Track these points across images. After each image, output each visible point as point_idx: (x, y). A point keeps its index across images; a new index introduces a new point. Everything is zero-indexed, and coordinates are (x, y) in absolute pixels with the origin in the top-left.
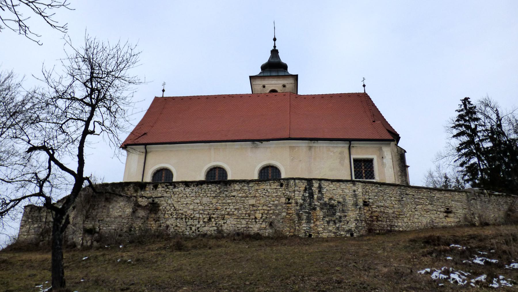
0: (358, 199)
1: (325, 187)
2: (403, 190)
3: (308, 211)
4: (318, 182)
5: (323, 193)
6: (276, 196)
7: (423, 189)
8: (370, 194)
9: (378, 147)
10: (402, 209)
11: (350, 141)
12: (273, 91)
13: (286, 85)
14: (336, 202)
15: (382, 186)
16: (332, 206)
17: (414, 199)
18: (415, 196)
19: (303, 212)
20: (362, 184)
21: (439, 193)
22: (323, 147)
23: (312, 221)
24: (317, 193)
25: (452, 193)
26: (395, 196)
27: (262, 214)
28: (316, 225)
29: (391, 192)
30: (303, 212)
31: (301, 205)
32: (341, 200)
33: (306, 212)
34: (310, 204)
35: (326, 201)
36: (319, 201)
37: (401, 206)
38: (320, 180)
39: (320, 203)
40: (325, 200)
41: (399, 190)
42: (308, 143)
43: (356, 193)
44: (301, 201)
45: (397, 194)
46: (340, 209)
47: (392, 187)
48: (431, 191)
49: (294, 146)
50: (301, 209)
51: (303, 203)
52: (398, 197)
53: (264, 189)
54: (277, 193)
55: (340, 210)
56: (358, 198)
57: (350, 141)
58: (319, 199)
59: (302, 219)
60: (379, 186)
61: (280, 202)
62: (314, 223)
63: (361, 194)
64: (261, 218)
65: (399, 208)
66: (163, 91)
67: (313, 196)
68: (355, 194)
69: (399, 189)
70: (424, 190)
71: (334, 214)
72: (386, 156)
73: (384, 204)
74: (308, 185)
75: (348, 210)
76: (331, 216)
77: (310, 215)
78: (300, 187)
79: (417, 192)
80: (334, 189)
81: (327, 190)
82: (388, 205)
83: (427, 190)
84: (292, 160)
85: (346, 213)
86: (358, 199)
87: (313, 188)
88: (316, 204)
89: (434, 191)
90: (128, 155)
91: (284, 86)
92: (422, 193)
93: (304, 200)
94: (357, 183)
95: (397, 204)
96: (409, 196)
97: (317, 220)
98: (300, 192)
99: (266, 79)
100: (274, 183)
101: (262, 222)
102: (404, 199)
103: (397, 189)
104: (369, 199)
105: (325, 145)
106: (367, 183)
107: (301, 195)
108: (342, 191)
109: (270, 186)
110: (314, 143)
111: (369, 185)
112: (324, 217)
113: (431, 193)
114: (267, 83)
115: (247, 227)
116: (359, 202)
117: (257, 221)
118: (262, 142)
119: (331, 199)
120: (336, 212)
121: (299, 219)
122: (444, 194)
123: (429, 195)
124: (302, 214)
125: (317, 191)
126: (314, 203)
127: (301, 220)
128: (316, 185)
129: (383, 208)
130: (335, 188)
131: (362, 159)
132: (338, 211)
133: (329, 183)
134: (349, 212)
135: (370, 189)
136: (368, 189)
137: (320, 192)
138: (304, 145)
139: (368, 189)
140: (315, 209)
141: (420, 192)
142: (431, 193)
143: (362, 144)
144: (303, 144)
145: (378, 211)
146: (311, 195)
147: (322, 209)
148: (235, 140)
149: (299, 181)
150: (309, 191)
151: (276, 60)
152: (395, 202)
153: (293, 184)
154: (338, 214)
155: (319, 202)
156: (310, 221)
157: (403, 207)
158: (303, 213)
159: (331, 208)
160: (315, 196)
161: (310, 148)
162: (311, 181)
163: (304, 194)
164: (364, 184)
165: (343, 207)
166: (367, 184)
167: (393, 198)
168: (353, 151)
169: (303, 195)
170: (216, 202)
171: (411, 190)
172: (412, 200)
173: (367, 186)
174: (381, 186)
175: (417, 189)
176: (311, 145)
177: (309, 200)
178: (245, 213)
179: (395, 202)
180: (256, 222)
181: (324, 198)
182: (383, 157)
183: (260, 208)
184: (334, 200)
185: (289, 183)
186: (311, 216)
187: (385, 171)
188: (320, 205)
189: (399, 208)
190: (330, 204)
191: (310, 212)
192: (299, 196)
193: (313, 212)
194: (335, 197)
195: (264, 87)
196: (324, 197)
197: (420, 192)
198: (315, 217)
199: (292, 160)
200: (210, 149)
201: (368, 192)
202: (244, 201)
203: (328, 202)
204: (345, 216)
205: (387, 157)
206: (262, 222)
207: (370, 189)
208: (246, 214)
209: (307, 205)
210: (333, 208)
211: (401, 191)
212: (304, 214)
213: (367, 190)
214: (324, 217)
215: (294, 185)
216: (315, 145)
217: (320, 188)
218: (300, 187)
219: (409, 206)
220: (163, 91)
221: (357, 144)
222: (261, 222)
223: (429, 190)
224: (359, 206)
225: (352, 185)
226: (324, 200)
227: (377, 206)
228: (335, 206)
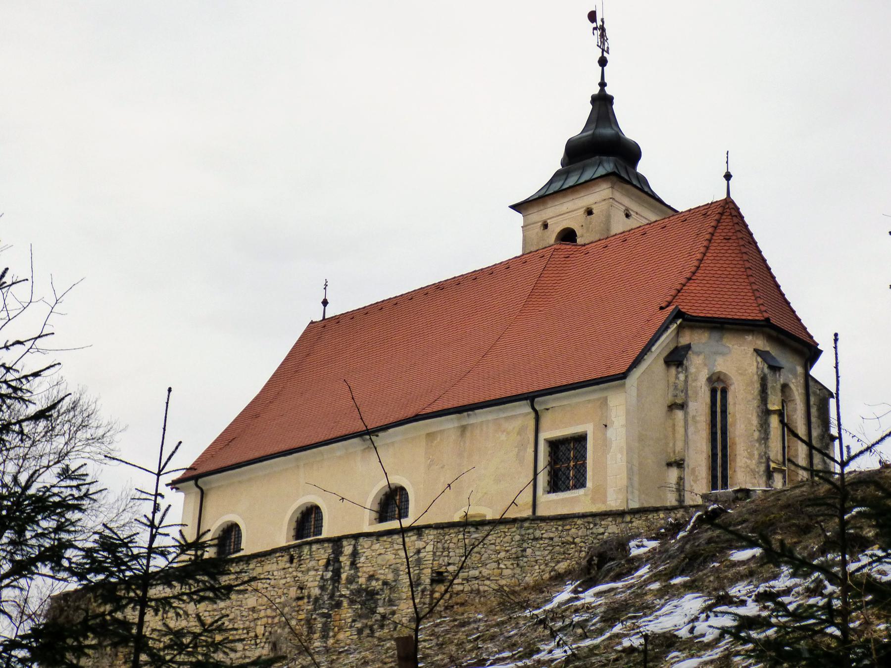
0: (423, 569)
1: (364, 552)
2: (528, 528)
3: (326, 611)
4: (353, 542)
5: (358, 565)
6: (284, 584)
7: (575, 520)
8: (451, 554)
9: (598, 399)
10: (520, 577)
11: (531, 397)
12: (568, 236)
13: (593, 207)
14: (380, 582)
15: (480, 528)
16: (372, 594)
17: (551, 548)
18: (556, 539)
19: (318, 614)
20: (435, 532)
21: (619, 520)
22: (488, 421)
23: (331, 634)
24: (347, 568)
25: (650, 516)
26: (507, 549)
27: (265, 627)
28: (338, 641)
29: (498, 541)
30: (318, 614)
31: (317, 599)
32: (390, 577)
33: (324, 615)
34: (332, 597)
35: (361, 585)
36: (349, 586)
37: (518, 571)
38: (356, 537)
39: (351, 591)
40: (360, 583)
41: (518, 532)
42: (459, 419)
43: (422, 555)
44: (316, 592)
45: (513, 543)
46: (384, 599)
47: (502, 527)
48: (597, 520)
49: (441, 431)
50: (315, 610)
51: (320, 594)
52: (514, 551)
53: (269, 572)
54: (285, 578)
55: (384, 601)
56: (423, 566)
57: (531, 397)
58: (351, 580)
59: (314, 630)
60: (472, 529)
61: (289, 597)
62: (334, 636)
63: (430, 557)
64: (264, 635)
65: (513, 576)
66: (325, 303)
67: (340, 577)
68: (419, 558)
69: (517, 528)
70: (579, 522)
71: (373, 611)
72: (613, 419)
73: (480, 573)
74: (333, 553)
75: (400, 599)
76: (367, 617)
77: (329, 620)
78: (318, 560)
79: (560, 528)
80: (380, 554)
81: (367, 559)
82: (490, 572)
83: (586, 520)
84: (430, 466)
85: (395, 606)
86: (423, 569)
87: (341, 559)
88: (343, 593)
89: (603, 520)
90: (185, 498)
91: (589, 212)
92: (573, 530)
93: (322, 588)
94: (427, 531)
95: (511, 567)
96: (541, 542)
97: (341, 629)
98: (317, 570)
99: (550, 204)
100: (282, 556)
101: (265, 643)
102: (529, 551)
103: (514, 529)
104: (449, 564)
105: (490, 417)
106: (447, 527)
107: (318, 578)
108: (396, 555)
109: (278, 564)
110: (469, 415)
111: (452, 531)
112: (354, 621)
113: (595, 525)
114: (551, 215)
115: (243, 656)
116: (423, 577)
117: (258, 641)
118: (376, 433)
119: (371, 577)
120: (376, 607)
121: (308, 633)
122: (631, 522)
123: (589, 532)
124: (315, 619)
125: (348, 563)
126: (340, 591)
127: (311, 633)
128: (348, 549)
129: (477, 582)
130: (383, 551)
131: (567, 438)
132: (380, 603)
133: (372, 542)
134: (402, 601)
135: (453, 541)
136: (448, 542)
137: (353, 564)
138: (450, 425)
139: (448, 542)
140: (339, 605)
141: (568, 527)
142: (595, 525)
143: (565, 398)
144: (449, 423)
145: (466, 589)
146: (337, 574)
147: (352, 602)
148: (655, 334)
149: (318, 546)
150: (333, 565)
151: (607, 131)
152: (506, 563)
153: (307, 555)
154: (381, 610)
155: (348, 588)
156: (328, 634)
157: (523, 571)
158: (317, 617)
159: (369, 598)
160: (344, 576)
161: (463, 429)
162: (339, 543)
163: (324, 574)
164: (439, 531)
165: (390, 594)
166: (447, 530)
167: (502, 554)
168: (545, 421)
169: (322, 578)
170: (204, 609)
171: (548, 527)
172: (547, 552)
173: (445, 534)
174: (477, 529)
175: (560, 523)
176: (464, 423)
177: (331, 587)
178: (242, 626)
179: (506, 563)
180: (256, 644)
181: (359, 577)
182: (606, 426)
183: (262, 614)
184: (377, 580)
185: (302, 554)
186: (331, 622)
187: (609, 462)
188: (350, 594)
189: (513, 576)
190: (369, 589)
191: (330, 614)
192: (315, 581)
193: (336, 611)
194: (380, 571)
195: (589, 212)
196: (360, 574)
197: (568, 527)
198: (337, 623)
199: (430, 466)
200: (298, 467)
201: (448, 548)
202: (241, 601)
203: (366, 584)
204: (393, 613)
205: (616, 424)
206: (265, 643)
207: (453, 541)
208: (243, 629)
209: (326, 599)
210: (372, 599)
211: (523, 532)
212: (319, 619)
213: (446, 545)
214: (354, 621)
215: (308, 557)
216: (472, 421)
217: (355, 554)
218: (318, 560)
219: (537, 567)
220: (325, 303)
221: (554, 399)
222: (262, 644)
223: (590, 519)
224: (423, 587)
225: (414, 538)
226: (358, 582)
227: (463, 579)
228: (377, 594)
